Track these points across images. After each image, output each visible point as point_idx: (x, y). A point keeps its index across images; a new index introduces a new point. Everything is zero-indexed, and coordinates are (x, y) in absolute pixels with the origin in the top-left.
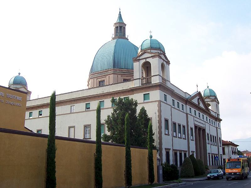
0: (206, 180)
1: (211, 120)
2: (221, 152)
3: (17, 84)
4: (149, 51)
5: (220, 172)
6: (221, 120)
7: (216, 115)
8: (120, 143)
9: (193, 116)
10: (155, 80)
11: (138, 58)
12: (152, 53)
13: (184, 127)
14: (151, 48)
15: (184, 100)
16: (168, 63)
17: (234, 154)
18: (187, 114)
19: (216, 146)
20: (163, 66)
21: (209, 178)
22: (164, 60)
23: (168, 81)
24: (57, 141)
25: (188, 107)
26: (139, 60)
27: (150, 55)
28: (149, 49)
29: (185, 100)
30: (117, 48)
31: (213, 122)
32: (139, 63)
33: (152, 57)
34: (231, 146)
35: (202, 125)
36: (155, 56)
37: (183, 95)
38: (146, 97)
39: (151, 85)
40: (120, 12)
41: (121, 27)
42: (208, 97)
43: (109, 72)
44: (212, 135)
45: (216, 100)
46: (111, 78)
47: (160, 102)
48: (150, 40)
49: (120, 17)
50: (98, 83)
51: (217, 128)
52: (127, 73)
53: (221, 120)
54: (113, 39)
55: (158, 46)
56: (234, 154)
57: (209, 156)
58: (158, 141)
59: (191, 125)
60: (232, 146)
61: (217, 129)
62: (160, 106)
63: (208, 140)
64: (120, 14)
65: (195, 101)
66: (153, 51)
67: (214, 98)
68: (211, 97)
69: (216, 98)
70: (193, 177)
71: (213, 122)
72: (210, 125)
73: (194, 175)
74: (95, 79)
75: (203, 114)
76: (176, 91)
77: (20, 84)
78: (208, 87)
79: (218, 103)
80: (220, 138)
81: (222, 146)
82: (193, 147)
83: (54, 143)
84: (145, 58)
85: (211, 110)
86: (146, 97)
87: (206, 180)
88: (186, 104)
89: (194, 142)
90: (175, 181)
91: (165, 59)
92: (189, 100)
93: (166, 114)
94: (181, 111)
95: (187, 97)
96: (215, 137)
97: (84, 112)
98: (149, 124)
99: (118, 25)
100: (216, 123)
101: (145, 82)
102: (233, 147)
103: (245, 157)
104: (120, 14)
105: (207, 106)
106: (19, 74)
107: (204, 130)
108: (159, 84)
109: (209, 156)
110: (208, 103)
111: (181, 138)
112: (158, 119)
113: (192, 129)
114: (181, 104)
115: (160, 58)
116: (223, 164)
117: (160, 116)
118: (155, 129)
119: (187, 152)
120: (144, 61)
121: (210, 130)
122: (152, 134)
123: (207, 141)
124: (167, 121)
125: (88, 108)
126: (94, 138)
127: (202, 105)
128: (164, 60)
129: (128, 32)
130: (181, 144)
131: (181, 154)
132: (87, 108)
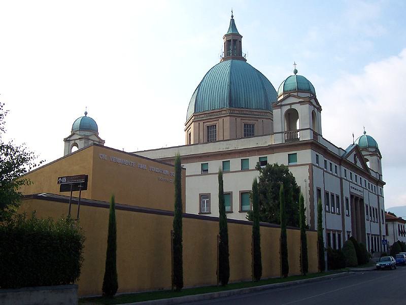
0: (375, 270)
1: (328, 162)
2: (384, 233)
3: (86, 129)
4: (296, 94)
5: (393, 260)
6: (385, 184)
7: (377, 175)
8: (271, 222)
9: (348, 181)
10: (305, 136)
11: (280, 104)
12: (299, 97)
13: (338, 197)
14: (299, 90)
15: (338, 158)
16: (320, 109)
17: (402, 235)
18: (341, 179)
19: (377, 223)
20: (313, 114)
21: (379, 268)
22: (314, 106)
23: (319, 135)
24: (229, 224)
25: (343, 168)
26: (281, 106)
27: (369, 153)
28: (294, 91)
29: (339, 159)
30: (234, 77)
31: (334, 167)
32: (281, 111)
33: (300, 102)
34: (397, 223)
35: (359, 193)
36: (303, 102)
37: (336, 152)
38: (292, 158)
39: (299, 142)
40: (232, 17)
41: (235, 41)
42: (365, 149)
43: (223, 112)
44: (330, 191)
45: (313, 101)
46: (224, 125)
47: (311, 165)
48: (297, 78)
49: (233, 24)
50: (206, 128)
51: (378, 195)
52: (250, 115)
53: (385, 184)
54: (224, 59)
55: (307, 87)
56: (402, 235)
57: (368, 237)
58: (310, 218)
59: (347, 194)
60: (399, 223)
61: (378, 198)
62: (311, 172)
63: (367, 214)
64: (233, 21)
65: (351, 159)
66: (300, 94)
67: (374, 150)
68: (370, 149)
69: (377, 150)
70: (355, 266)
71: (334, 167)
72: (326, 172)
73: (357, 264)
74: (201, 123)
75: (318, 154)
76: (330, 148)
77: (88, 129)
78: (365, 133)
79: (318, 109)
80: (382, 211)
81: (386, 221)
82: (348, 227)
83: (226, 226)
84: (291, 104)
85: (372, 170)
86: (292, 158)
87: (375, 270)
88: (340, 165)
89: (350, 218)
90: (343, 270)
91: (316, 105)
92: (344, 159)
93: (318, 183)
94: (329, 173)
95: (342, 153)
96: (376, 210)
97: (199, 175)
98: (300, 196)
99: (230, 38)
100: (340, 169)
101: (287, 137)
102: (400, 224)
103: (3, 224)
104: (233, 21)
105: (364, 162)
106: (86, 113)
107: (362, 200)
108: (311, 141)
109: (368, 237)
110: (365, 157)
111: (334, 213)
112: (309, 189)
113: (347, 200)
114: (334, 164)
115: (311, 104)
116: (386, 251)
117: (311, 185)
118: (307, 204)
119: (342, 233)
120: (288, 107)
121: (369, 200)
122: (303, 210)
123: (366, 217)
124: (319, 191)
125: (205, 171)
126: (215, 213)
127: (359, 164)
128: (314, 106)
129: (248, 49)
130: (333, 221)
131: (334, 235)
132: (204, 171)
